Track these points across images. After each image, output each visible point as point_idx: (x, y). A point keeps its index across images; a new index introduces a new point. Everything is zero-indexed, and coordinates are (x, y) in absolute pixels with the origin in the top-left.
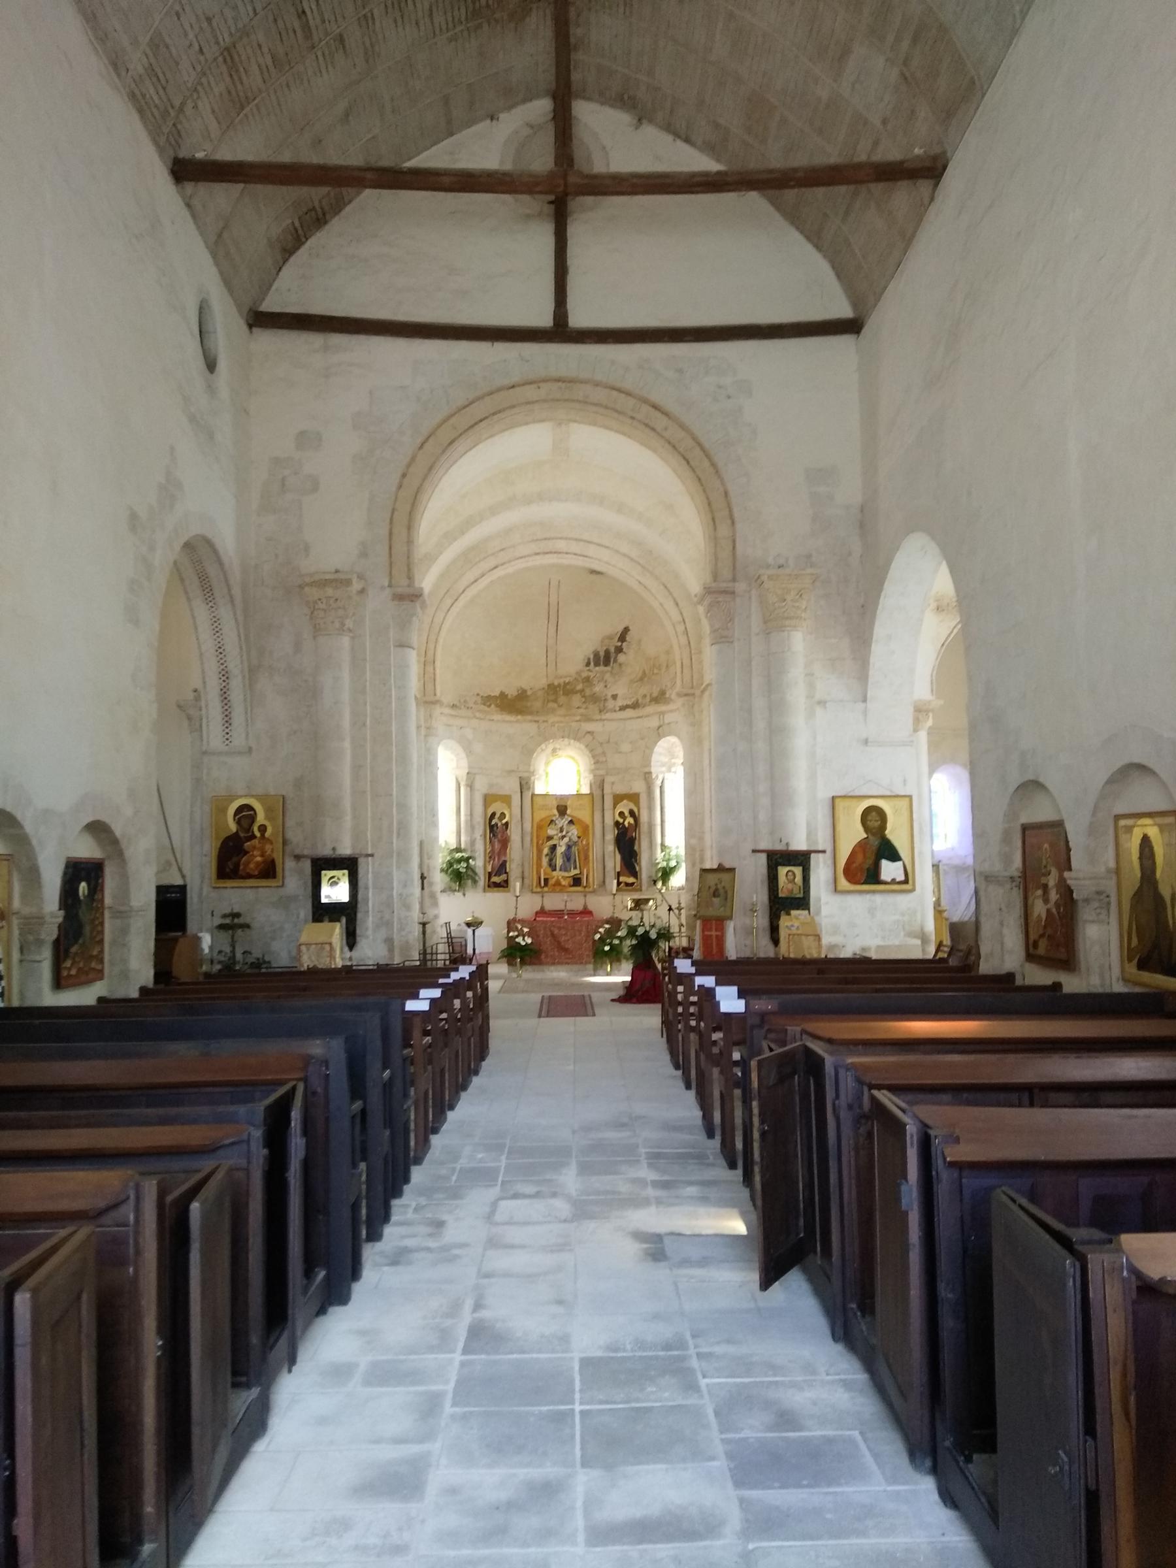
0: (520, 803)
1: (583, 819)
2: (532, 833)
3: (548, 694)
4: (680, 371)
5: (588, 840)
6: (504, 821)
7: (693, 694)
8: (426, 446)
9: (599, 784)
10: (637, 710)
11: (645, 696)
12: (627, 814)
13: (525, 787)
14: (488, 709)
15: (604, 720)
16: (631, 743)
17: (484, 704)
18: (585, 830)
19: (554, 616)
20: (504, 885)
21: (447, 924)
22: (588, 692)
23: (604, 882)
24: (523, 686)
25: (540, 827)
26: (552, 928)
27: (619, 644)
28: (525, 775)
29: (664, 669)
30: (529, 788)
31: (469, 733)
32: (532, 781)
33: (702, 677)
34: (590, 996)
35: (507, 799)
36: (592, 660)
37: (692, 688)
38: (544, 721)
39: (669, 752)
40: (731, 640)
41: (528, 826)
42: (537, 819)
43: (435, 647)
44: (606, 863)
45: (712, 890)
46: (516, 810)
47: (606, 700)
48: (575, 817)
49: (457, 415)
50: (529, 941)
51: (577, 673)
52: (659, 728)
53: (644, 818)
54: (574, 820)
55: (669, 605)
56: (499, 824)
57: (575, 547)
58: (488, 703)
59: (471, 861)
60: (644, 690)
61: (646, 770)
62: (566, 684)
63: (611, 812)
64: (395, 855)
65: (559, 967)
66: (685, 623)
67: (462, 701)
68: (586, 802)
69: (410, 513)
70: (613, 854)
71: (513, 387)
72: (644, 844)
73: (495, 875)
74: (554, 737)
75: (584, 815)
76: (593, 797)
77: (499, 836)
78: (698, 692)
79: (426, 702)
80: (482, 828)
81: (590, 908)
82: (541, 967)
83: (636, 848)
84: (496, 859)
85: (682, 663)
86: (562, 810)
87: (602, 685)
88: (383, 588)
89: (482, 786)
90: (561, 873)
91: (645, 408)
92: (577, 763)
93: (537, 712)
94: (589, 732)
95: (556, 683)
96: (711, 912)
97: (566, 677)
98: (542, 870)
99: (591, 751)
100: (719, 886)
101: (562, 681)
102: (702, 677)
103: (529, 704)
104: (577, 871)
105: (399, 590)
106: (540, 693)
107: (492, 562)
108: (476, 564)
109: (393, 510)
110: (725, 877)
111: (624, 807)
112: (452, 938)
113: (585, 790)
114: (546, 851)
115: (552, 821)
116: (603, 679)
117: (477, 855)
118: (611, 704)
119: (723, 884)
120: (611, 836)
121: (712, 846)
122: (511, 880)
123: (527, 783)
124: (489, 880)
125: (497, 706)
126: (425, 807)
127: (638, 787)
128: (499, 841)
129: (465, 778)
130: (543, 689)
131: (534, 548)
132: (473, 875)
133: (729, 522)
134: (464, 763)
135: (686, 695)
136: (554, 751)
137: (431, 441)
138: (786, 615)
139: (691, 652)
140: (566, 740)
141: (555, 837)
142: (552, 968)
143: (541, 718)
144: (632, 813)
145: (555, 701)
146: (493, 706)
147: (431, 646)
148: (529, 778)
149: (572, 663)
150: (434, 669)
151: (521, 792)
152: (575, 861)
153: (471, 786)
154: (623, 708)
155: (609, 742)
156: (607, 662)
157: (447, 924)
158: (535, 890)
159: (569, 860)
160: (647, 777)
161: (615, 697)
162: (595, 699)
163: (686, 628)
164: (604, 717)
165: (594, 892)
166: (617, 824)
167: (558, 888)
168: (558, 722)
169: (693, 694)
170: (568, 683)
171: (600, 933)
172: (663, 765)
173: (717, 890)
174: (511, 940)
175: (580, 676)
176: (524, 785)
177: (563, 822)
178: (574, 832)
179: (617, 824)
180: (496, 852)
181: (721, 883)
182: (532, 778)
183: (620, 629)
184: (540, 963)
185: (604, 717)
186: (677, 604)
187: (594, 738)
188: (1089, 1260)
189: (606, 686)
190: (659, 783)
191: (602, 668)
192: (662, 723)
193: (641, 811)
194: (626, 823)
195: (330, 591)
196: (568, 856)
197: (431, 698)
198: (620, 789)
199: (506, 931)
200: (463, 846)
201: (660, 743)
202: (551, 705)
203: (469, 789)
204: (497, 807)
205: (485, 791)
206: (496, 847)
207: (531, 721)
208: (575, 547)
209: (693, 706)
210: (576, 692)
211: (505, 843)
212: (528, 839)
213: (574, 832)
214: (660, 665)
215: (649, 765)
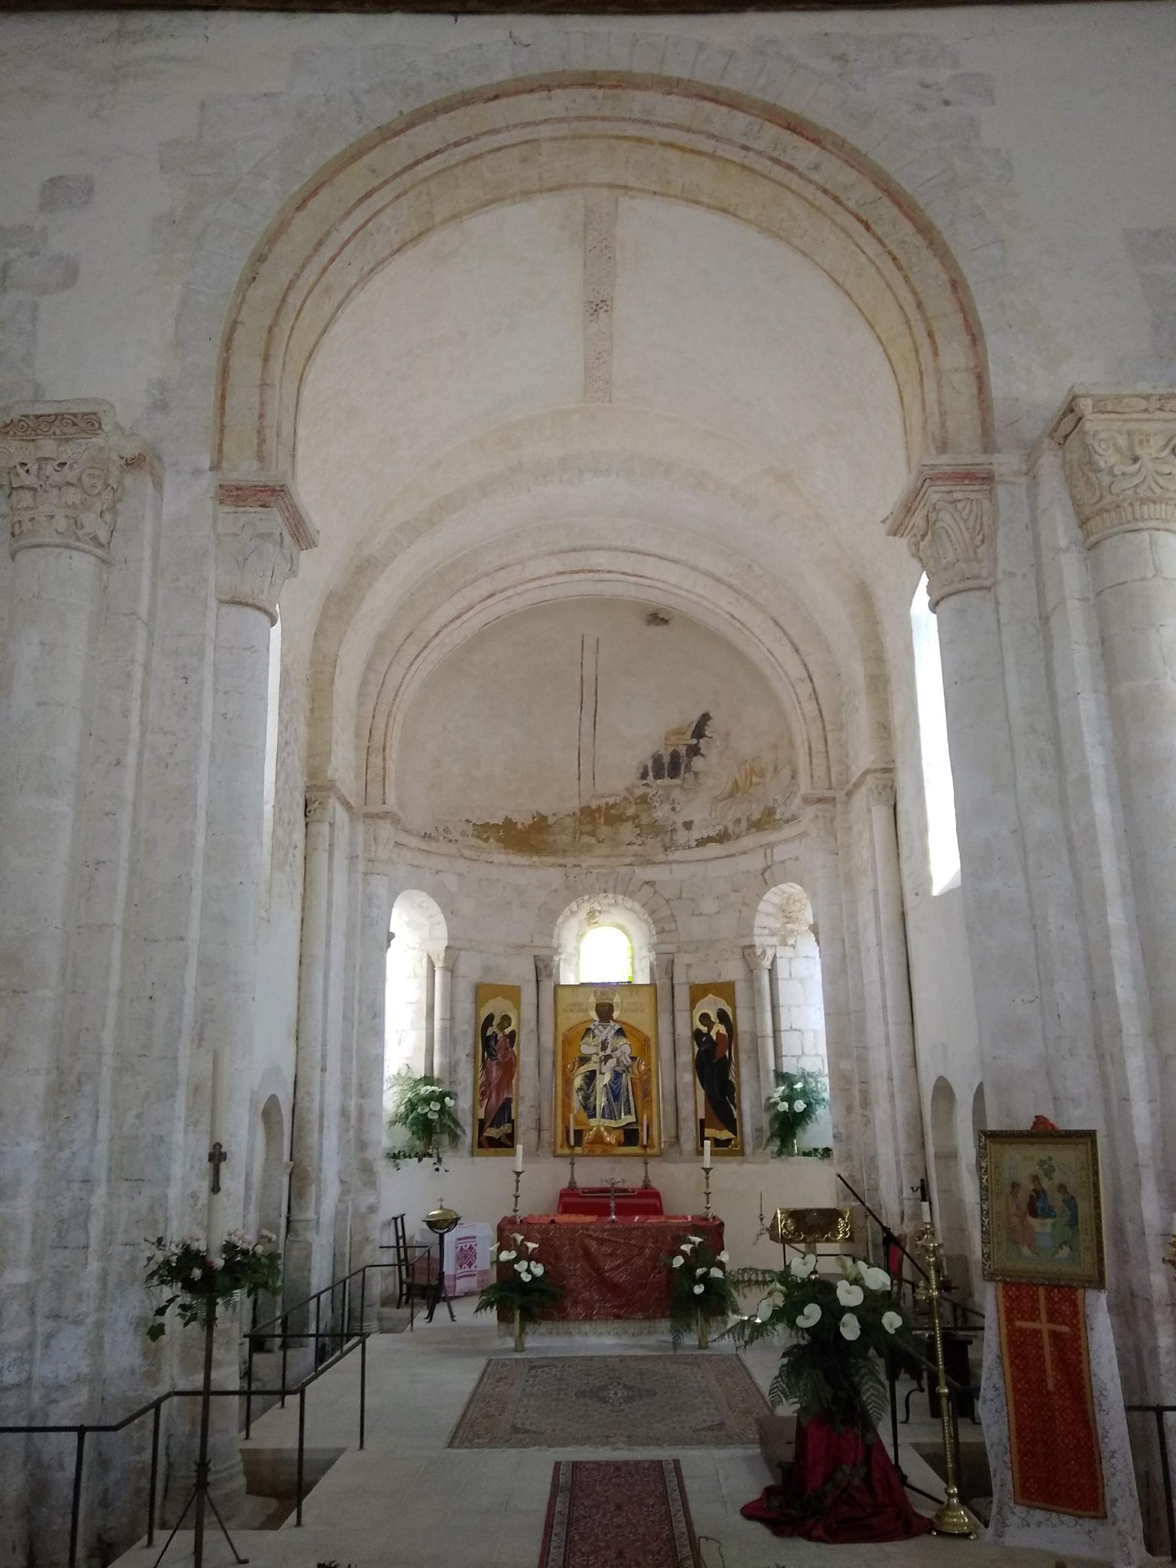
0: (536, 1001)
1: (641, 1028)
2: (555, 1053)
3: (581, 823)
4: (842, 58)
5: (648, 1064)
6: (507, 1031)
7: (834, 799)
8: (314, 204)
9: (665, 967)
10: (726, 845)
11: (738, 821)
12: (714, 1018)
13: (543, 973)
14: (484, 845)
15: (671, 863)
17: (478, 837)
18: (644, 1045)
20: (506, 1143)
21: (398, 1221)
22: (645, 819)
23: (677, 1137)
25: (568, 1041)
26: (587, 1241)
27: (694, 741)
28: (543, 952)
29: (769, 775)
30: (550, 975)
31: (451, 881)
32: (556, 963)
33: (848, 768)
34: (677, 1462)
35: (512, 993)
36: (650, 770)
38: (575, 866)
40: (987, 583)
41: (547, 1039)
42: (562, 1029)
44: (680, 1103)
45: (1023, 1197)
46: (528, 1012)
47: (674, 831)
48: (624, 1023)
49: (379, 148)
50: (539, 1270)
51: (627, 789)
52: (765, 870)
53: (743, 1025)
54: (625, 1028)
55: (784, 653)
56: (500, 1035)
57: (624, 563)
58: (485, 836)
59: (447, 1099)
60: (737, 811)
61: (746, 942)
62: (610, 807)
63: (687, 1014)
64: (182, 1093)
65: (601, 1327)
66: (811, 680)
67: (441, 829)
68: (645, 998)
69: (270, 330)
70: (691, 1089)
71: (497, 97)
72: (746, 1072)
73: (491, 1126)
74: (591, 891)
75: (641, 1020)
76: (656, 991)
77: (499, 1056)
78: (840, 795)
79: (367, 816)
80: (470, 1041)
81: (656, 1184)
82: (561, 1326)
83: (732, 1077)
84: (494, 1095)
85: (810, 748)
86: (605, 1012)
87: (667, 807)
88: (196, 472)
89: (471, 969)
90: (603, 1120)
91: (772, 131)
92: (628, 935)
93: (565, 851)
94: (647, 883)
95: (594, 806)
96: (1025, 1260)
97: (610, 796)
98: (571, 1115)
99: (652, 913)
100: (1045, 1184)
101: (603, 802)
103: (551, 839)
104: (631, 1118)
105: (234, 477)
106: (569, 821)
107: (485, 587)
108: (459, 590)
109: (235, 324)
110: (1066, 1157)
111: (710, 1005)
112: (405, 1247)
113: (643, 979)
114: (578, 1082)
115: (588, 1030)
116: (668, 798)
117: (458, 1089)
118: (682, 836)
119: (1058, 1177)
120: (686, 1058)
121: (890, 1073)
122: (520, 1131)
123: (546, 967)
124: (480, 1134)
125: (499, 840)
126: (360, 1001)
127: (732, 971)
128: (498, 1064)
129: (442, 955)
130: (574, 814)
131: (555, 564)
132: (453, 1126)
133: (967, 339)
134: (442, 931)
135: (819, 801)
136: (592, 914)
137: (324, 194)
138: (1141, 492)
139: (824, 727)
141: (595, 1058)
142: (587, 1327)
143: (570, 861)
144: (722, 1016)
145: (592, 834)
146: (492, 840)
147: (381, 721)
148: (551, 958)
150: (384, 759)
151: (538, 982)
152: (628, 1100)
153: (451, 969)
154: (702, 843)
155: (680, 898)
157: (398, 1221)
158: (559, 1151)
159: (616, 1097)
160: (748, 954)
161: (688, 825)
162: (656, 829)
163: (814, 689)
164: (671, 857)
165: (660, 1155)
166: (697, 1034)
167: (599, 1149)
169: (834, 799)
170: (614, 806)
171: (683, 1253)
173: (1038, 1194)
174: (505, 1269)
175: (631, 793)
176: (543, 969)
177: (607, 1032)
178: (625, 1047)
179: (697, 1034)
180: (495, 1082)
181: (1049, 1173)
182: (556, 958)
183: (695, 717)
184: (564, 1317)
185: (671, 857)
186: (797, 651)
187: (655, 892)
189: (673, 809)
191: (667, 781)
192: (769, 864)
193: (739, 1012)
194: (713, 1034)
195: (48, 447)
196: (614, 1091)
198: (701, 976)
199: (494, 1247)
200: (436, 1074)
201: (768, 896)
202: (586, 839)
203: (449, 974)
204: (497, 1006)
205: (476, 977)
206: (494, 1075)
207: (552, 865)
208: (624, 563)
209: (832, 820)
210: (627, 819)
211: (509, 1067)
212: (548, 1060)
213: (625, 1047)
214: (762, 770)
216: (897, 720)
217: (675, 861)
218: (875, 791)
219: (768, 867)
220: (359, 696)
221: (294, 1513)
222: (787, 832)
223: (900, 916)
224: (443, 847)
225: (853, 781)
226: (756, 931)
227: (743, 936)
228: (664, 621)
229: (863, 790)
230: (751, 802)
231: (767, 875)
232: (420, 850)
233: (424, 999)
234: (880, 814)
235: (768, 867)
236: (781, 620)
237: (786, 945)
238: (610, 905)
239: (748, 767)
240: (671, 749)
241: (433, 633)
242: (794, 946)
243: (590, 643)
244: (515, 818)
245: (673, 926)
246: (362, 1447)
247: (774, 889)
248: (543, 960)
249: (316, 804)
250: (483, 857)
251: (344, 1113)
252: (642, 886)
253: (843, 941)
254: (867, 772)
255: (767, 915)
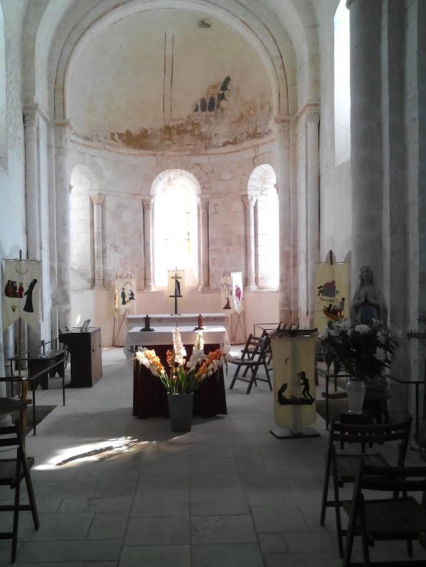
3: (165, 134)
10: (236, 146)
16: (231, 172)
19: (169, 68)
23: (209, 283)
24: (145, 127)
27: (222, 92)
31: (100, 161)
37: (288, 115)
39: (262, 178)
43: (64, 76)
47: (210, 138)
51: (188, 117)
52: (254, 158)
61: (243, 193)
74: (169, 167)
94: (197, 164)
101: (175, 123)
102: (296, 106)
118: (214, 141)
125: (124, 141)
129: (97, 197)
134: (96, 186)
140: (179, 170)
145: (170, 139)
149: (183, 108)
151: (144, 212)
154: (225, 145)
156: (211, 109)
162: (201, 137)
168: (172, 156)
169: (289, 121)
170: (181, 125)
172: (257, 189)
182: (152, 201)
183: (223, 80)
185: (209, 152)
186: (275, 42)
188: (354, 413)
190: (253, 203)
197: (59, 121)
202: (167, 142)
207: (150, 155)
210: (187, 132)
215: (246, 190)
216: (323, 79)
217: (211, 154)
218: (310, 116)
219: (256, 156)
220: (49, 60)
221: (33, 431)
222: (266, 139)
223: (317, 178)
224: (95, 144)
225: (300, 111)
226: (249, 188)
227: (242, 190)
228: (208, 26)
229: (304, 116)
230: (249, 124)
231: (255, 160)
232: (84, 145)
233: (89, 218)
234: (312, 127)
235: (256, 156)
236: (268, 25)
237: (262, 195)
238: (179, 175)
239: (248, 106)
240: (210, 96)
241: (87, 26)
242: (266, 195)
243: (169, 37)
244: (131, 130)
245: (209, 185)
246: (64, 405)
247: (258, 167)
248: (146, 201)
249: (29, 117)
250: (116, 149)
251: (52, 269)
252: (194, 166)
253: (290, 191)
254: (307, 105)
255: (255, 180)
